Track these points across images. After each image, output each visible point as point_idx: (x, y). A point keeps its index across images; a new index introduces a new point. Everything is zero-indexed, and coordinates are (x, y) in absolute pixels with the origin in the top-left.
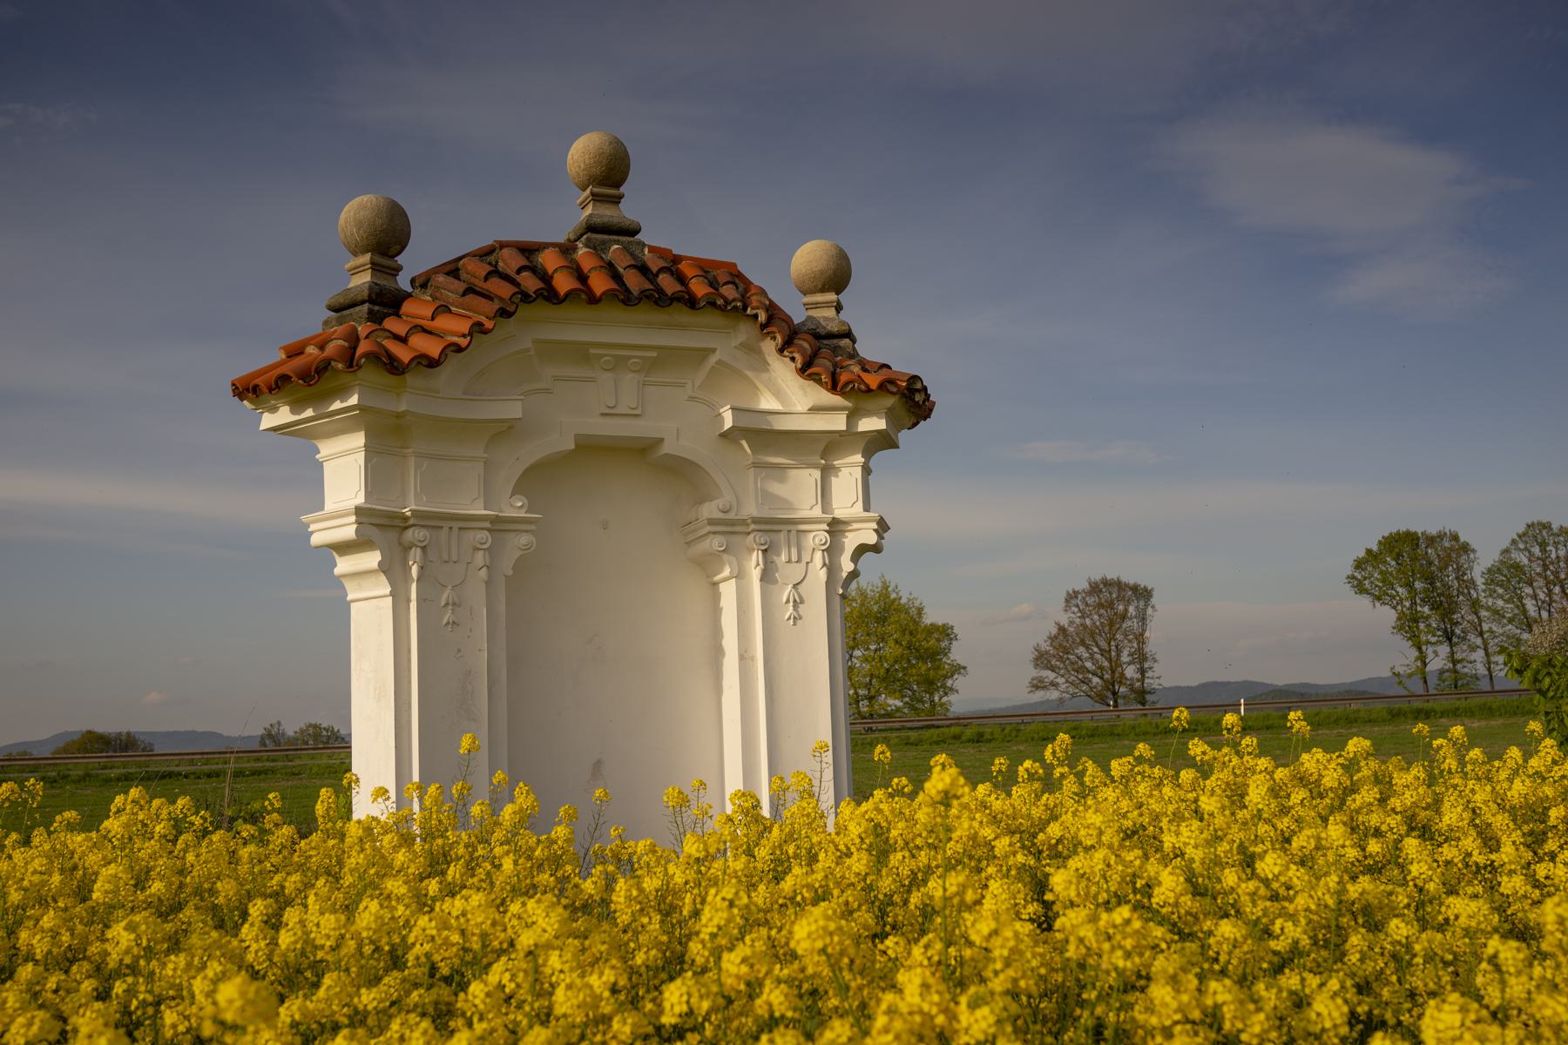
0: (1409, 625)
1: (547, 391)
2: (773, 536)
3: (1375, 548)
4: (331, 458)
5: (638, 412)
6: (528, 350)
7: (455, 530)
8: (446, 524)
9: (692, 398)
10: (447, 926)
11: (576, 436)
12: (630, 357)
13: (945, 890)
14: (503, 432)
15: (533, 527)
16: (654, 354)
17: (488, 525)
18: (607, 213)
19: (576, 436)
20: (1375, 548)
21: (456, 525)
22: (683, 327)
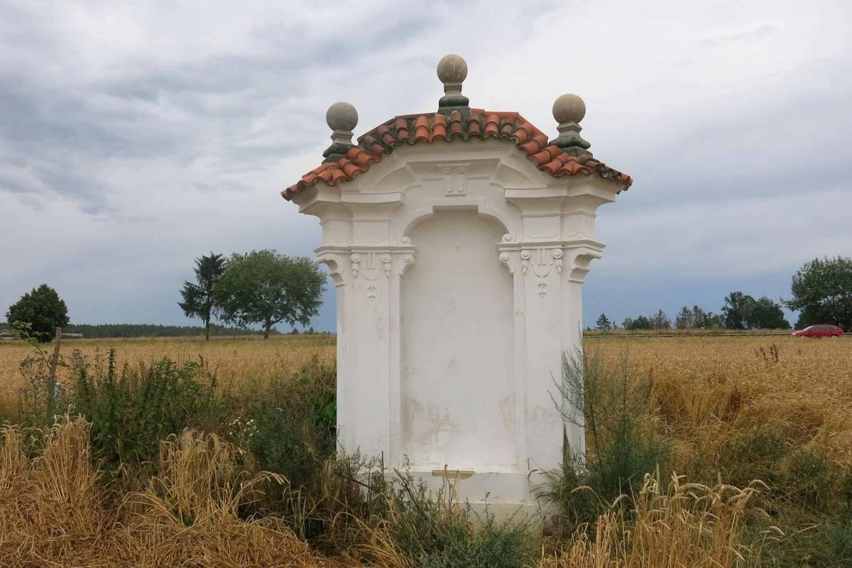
0: (795, 325)
1: (419, 186)
2: (533, 252)
3: (37, 290)
4: (358, 221)
5: (463, 193)
6: (405, 168)
7: (374, 255)
8: (369, 252)
9: (492, 184)
10: (791, 385)
11: (434, 207)
12: (444, 167)
13: (366, 486)
14: (396, 208)
15: (412, 251)
16: (469, 164)
17: (389, 251)
18: (453, 95)
19: (434, 207)
20: (37, 290)
21: (373, 252)
22: (481, 150)
